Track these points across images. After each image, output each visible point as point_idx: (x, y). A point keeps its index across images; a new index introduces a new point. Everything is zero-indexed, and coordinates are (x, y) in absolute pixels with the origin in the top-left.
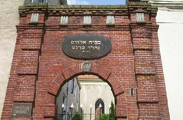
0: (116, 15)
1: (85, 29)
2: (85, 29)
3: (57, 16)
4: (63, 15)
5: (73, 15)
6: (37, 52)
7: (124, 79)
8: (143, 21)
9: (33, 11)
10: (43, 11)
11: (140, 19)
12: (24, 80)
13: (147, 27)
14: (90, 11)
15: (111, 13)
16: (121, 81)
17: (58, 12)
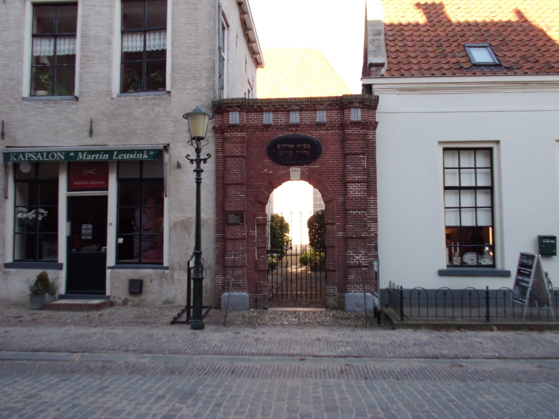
0: (331, 110)
4: (266, 111)
9: (230, 109)
15: (321, 107)
17: (259, 107)
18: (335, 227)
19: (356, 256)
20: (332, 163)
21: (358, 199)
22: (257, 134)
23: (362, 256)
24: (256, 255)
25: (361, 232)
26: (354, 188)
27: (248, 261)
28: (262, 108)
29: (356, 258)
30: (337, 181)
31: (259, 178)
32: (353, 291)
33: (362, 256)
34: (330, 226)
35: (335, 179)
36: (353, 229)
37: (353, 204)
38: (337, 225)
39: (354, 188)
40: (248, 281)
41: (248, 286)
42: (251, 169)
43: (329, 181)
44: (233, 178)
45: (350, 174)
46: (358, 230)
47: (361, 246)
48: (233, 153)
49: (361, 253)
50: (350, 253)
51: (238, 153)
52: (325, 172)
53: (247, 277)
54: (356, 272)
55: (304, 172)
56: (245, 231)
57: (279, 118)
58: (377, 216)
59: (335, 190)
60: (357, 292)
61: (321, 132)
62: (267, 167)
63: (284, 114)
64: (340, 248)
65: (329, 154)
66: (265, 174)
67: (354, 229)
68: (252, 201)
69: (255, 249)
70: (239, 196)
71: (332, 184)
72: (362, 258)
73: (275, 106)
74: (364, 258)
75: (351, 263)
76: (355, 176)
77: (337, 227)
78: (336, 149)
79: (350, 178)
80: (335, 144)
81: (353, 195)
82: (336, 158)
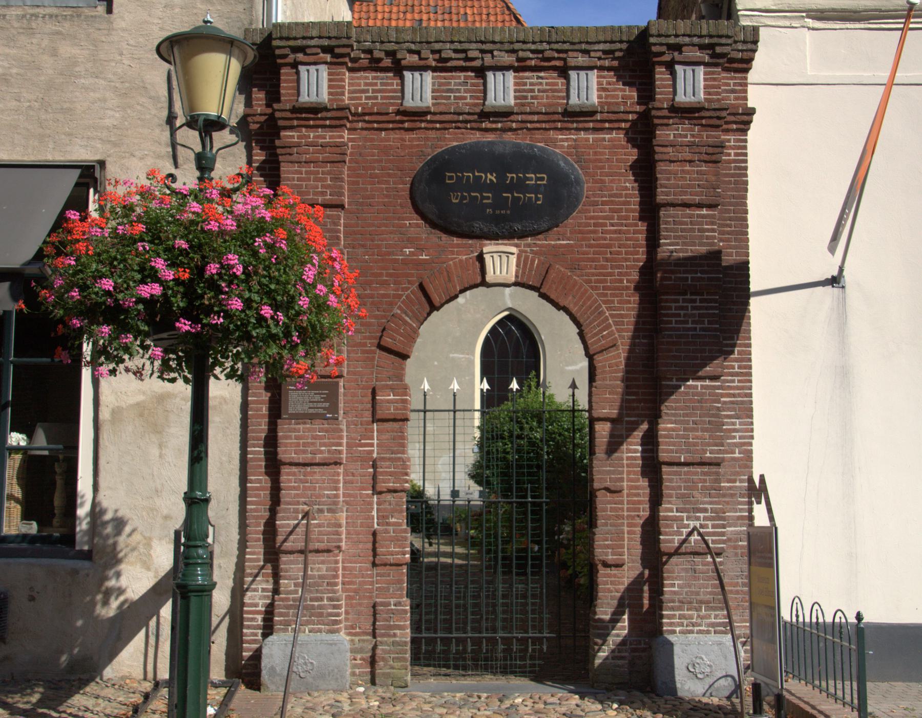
19: (688, 518)
20: (615, 232)
22: (382, 140)
23: (705, 518)
24: (375, 513)
25: (703, 444)
26: (682, 308)
29: (687, 526)
31: (388, 275)
32: (678, 629)
33: (705, 518)
35: (621, 281)
36: (678, 436)
39: (682, 308)
40: (348, 598)
41: (347, 613)
42: (363, 246)
43: (605, 288)
46: (697, 438)
47: (703, 488)
49: (705, 510)
51: (323, 194)
52: (593, 260)
54: (686, 570)
55: (526, 258)
58: (750, 395)
59: (621, 316)
60: (691, 632)
61: (582, 135)
63: (466, 77)
65: (604, 203)
67: (683, 437)
68: (365, 345)
71: (613, 295)
72: (706, 526)
73: (439, 52)
74: (713, 526)
81: (678, 329)
82: (627, 218)
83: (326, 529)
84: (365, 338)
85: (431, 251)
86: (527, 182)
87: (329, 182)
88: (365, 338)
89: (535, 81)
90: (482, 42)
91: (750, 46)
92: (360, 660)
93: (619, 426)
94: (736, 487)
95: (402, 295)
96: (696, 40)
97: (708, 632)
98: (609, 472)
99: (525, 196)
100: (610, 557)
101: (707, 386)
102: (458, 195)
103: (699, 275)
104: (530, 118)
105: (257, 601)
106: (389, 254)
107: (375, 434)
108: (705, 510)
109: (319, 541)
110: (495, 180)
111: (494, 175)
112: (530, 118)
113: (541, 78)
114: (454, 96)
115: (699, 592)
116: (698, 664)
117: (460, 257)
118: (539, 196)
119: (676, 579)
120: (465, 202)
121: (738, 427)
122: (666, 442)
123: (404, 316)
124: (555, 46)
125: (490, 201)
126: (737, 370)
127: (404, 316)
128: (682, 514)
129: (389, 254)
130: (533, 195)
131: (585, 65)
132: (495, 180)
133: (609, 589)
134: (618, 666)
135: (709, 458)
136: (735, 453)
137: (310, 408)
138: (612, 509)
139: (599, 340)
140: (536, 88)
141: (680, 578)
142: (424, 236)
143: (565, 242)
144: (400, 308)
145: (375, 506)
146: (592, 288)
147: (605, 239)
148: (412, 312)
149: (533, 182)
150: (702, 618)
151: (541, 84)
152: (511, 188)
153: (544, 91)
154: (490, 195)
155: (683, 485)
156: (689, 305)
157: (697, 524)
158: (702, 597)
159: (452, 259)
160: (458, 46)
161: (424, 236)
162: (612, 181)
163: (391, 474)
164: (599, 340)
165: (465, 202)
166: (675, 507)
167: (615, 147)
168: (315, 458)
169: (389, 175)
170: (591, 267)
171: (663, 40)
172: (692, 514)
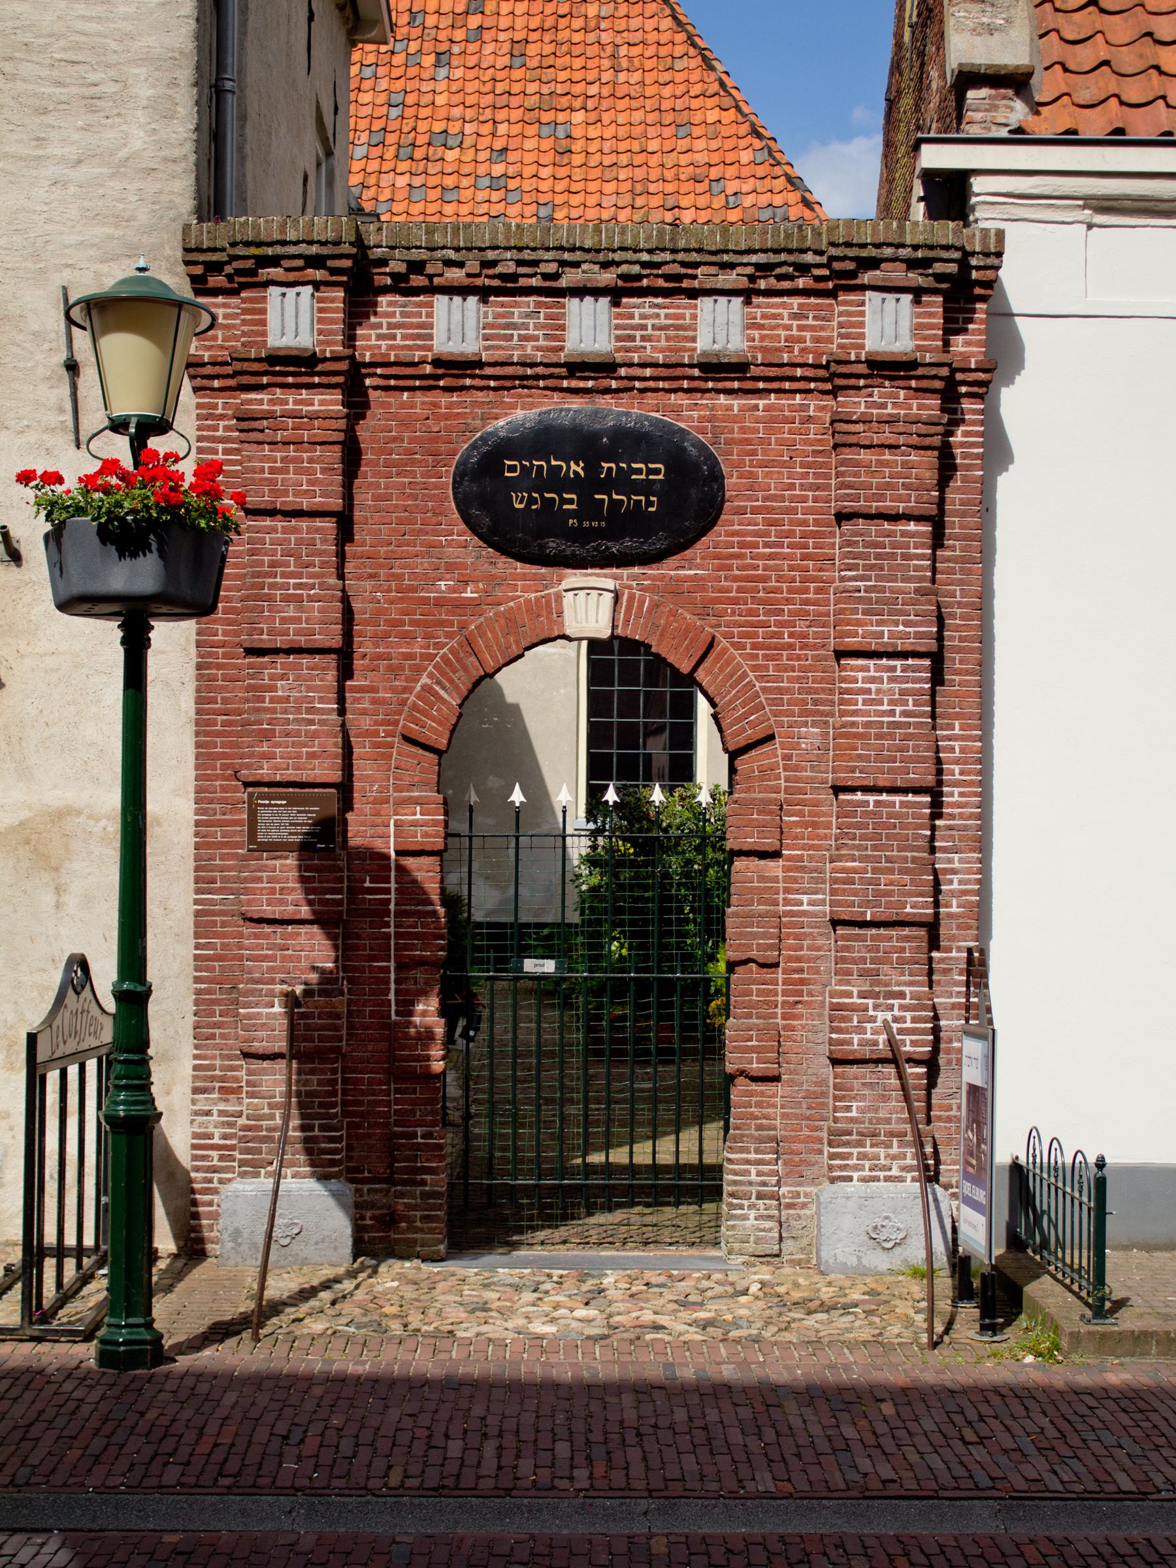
1: (574, 384)
2: (574, 384)
3: (417, 291)
4: (450, 290)
5: (509, 287)
6: (329, 525)
7: (778, 668)
8: (58, 1071)
10: (334, 271)
11: (889, 331)
12: (283, 677)
13: (925, 384)
14: (605, 265)
16: (760, 678)
17: (417, 267)
18: (774, 868)
19: (876, 1007)
20: (771, 557)
21: (891, 736)
22: (403, 405)
23: (902, 1008)
24: (392, 996)
26: (873, 680)
27: (351, 1026)
28: (430, 269)
29: (873, 1020)
30: (791, 647)
31: (413, 623)
32: (855, 1175)
33: (902, 1008)
34: (755, 863)
35: (780, 635)
37: (866, 758)
38: (790, 858)
39: (873, 680)
42: (372, 576)
43: (755, 646)
44: (284, 620)
45: (855, 611)
46: (891, 883)
48: (285, 493)
49: (902, 995)
50: (849, 995)
52: (735, 601)
53: (344, 1103)
55: (631, 597)
56: (340, 880)
57: (514, 326)
59: (781, 691)
60: (876, 1179)
62: (451, 567)
63: (538, 305)
64: (801, 971)
66: (439, 603)
68: (376, 734)
69: (387, 970)
70: (310, 710)
73: (493, 264)
75: (849, 1042)
76: (879, 623)
77: (786, 869)
78: (792, 487)
79: (856, 635)
80: (783, 464)
81: (867, 714)
83: (316, 1021)
84: (376, 723)
85: (481, 585)
86: (634, 477)
87: (319, 476)
88: (376, 723)
89: (647, 310)
90: (561, 248)
91: (991, 261)
92: (370, 1219)
93: (772, 864)
94: (951, 959)
95: (436, 655)
96: (903, 253)
97: (900, 1179)
98: (754, 936)
99: (629, 499)
100: (755, 1065)
101: (910, 802)
102: (523, 497)
103: (901, 628)
104: (638, 372)
105: (211, 1129)
106: (414, 589)
107: (393, 874)
108: (902, 995)
109: (305, 1040)
110: (582, 474)
111: (582, 465)
112: (638, 372)
113: (657, 306)
114: (519, 335)
115: (890, 1118)
116: (883, 1226)
117: (526, 595)
118: (652, 499)
119: (854, 1098)
120: (534, 507)
121: (956, 865)
122: (844, 890)
123: (437, 688)
124: (681, 256)
125: (574, 507)
126: (957, 777)
127: (437, 688)
128: (866, 1001)
129: (414, 589)
130: (642, 498)
131: (728, 286)
132: (582, 474)
133: (751, 1114)
134: (763, 1230)
135: (908, 914)
136: (951, 906)
137: (291, 834)
138: (760, 993)
139: (743, 730)
140: (649, 322)
141: (863, 1098)
142: (469, 561)
143: (692, 572)
144: (431, 676)
145: (393, 986)
146: (733, 644)
147: (756, 568)
148: (451, 681)
149: (643, 477)
150: (894, 1158)
151: (658, 316)
152: (607, 485)
153: (661, 328)
154: (574, 496)
155: (868, 955)
156: (885, 675)
157: (889, 1016)
158: (894, 1126)
159: (513, 599)
160: (527, 255)
161: (469, 561)
162: (767, 475)
163: (417, 936)
164: (743, 730)
165: (534, 507)
166: (855, 990)
167: (773, 420)
168: (300, 911)
169: (413, 462)
170: (733, 613)
171: (851, 252)
172: (881, 1001)
